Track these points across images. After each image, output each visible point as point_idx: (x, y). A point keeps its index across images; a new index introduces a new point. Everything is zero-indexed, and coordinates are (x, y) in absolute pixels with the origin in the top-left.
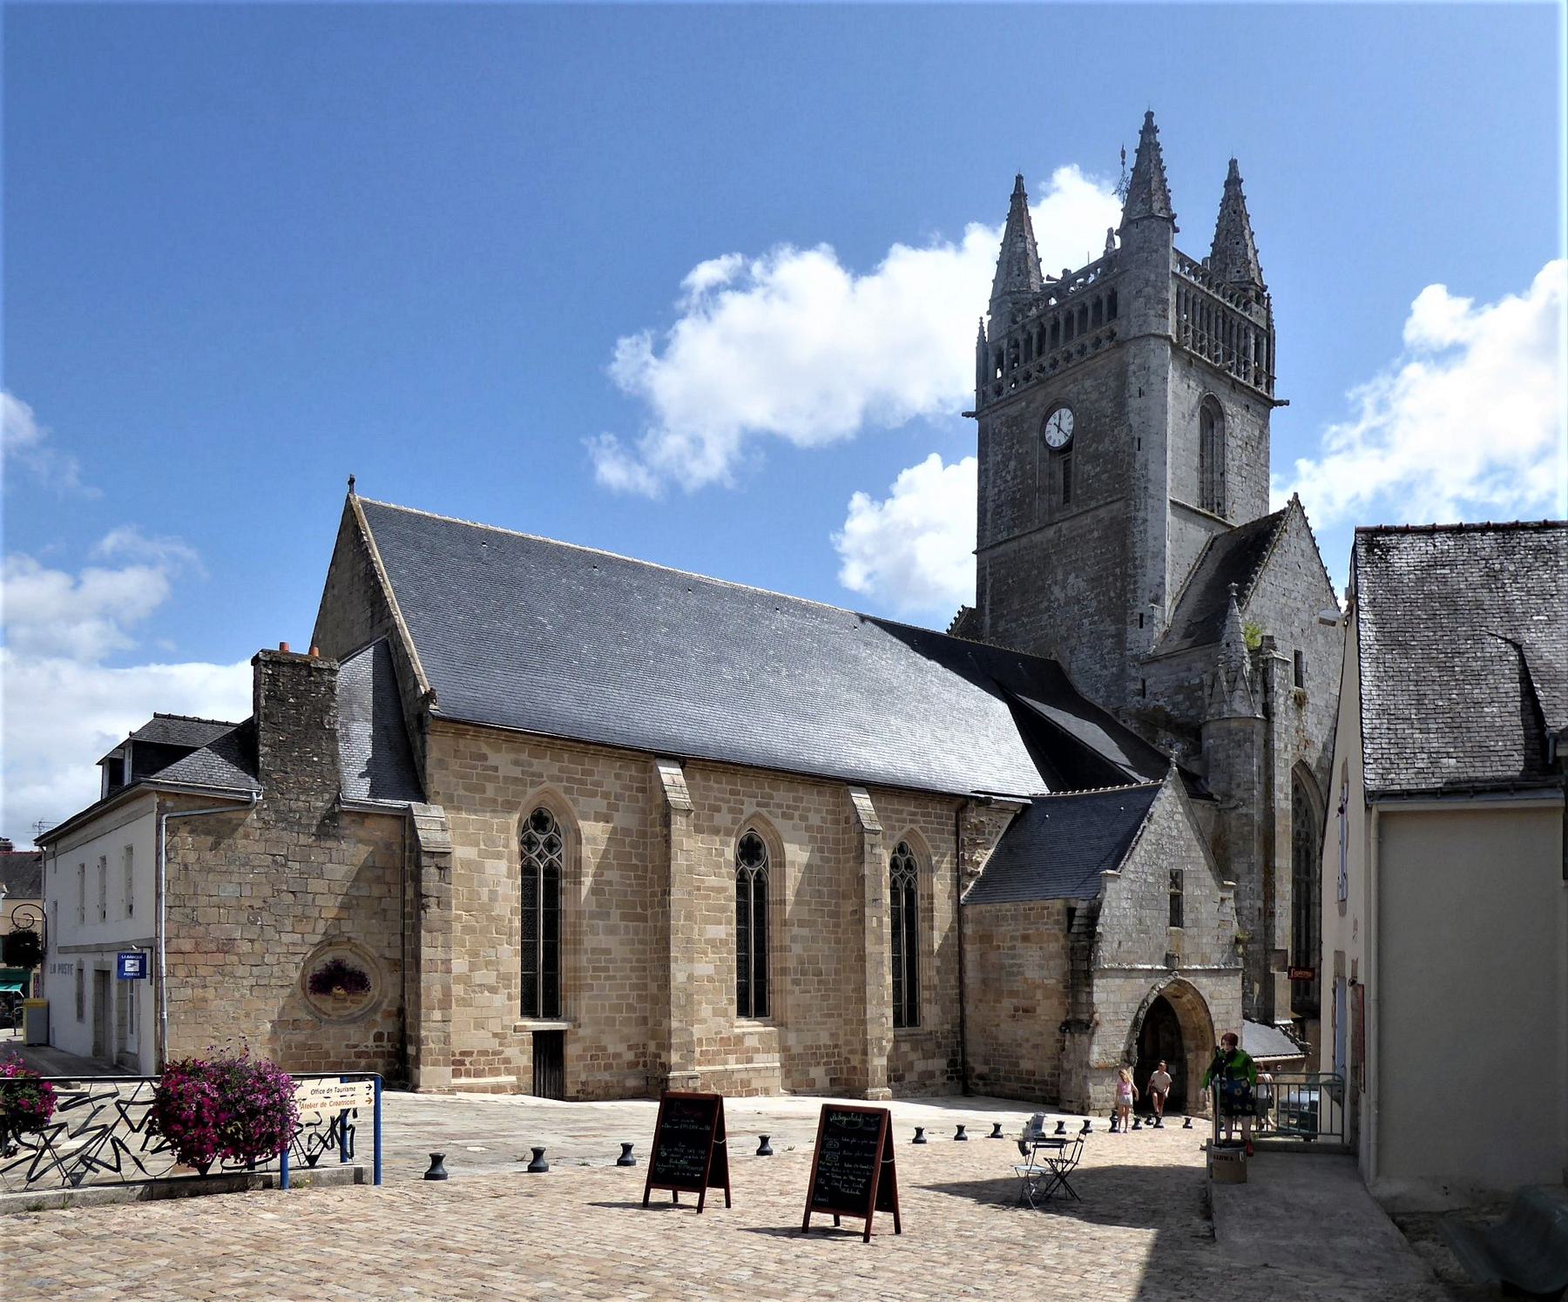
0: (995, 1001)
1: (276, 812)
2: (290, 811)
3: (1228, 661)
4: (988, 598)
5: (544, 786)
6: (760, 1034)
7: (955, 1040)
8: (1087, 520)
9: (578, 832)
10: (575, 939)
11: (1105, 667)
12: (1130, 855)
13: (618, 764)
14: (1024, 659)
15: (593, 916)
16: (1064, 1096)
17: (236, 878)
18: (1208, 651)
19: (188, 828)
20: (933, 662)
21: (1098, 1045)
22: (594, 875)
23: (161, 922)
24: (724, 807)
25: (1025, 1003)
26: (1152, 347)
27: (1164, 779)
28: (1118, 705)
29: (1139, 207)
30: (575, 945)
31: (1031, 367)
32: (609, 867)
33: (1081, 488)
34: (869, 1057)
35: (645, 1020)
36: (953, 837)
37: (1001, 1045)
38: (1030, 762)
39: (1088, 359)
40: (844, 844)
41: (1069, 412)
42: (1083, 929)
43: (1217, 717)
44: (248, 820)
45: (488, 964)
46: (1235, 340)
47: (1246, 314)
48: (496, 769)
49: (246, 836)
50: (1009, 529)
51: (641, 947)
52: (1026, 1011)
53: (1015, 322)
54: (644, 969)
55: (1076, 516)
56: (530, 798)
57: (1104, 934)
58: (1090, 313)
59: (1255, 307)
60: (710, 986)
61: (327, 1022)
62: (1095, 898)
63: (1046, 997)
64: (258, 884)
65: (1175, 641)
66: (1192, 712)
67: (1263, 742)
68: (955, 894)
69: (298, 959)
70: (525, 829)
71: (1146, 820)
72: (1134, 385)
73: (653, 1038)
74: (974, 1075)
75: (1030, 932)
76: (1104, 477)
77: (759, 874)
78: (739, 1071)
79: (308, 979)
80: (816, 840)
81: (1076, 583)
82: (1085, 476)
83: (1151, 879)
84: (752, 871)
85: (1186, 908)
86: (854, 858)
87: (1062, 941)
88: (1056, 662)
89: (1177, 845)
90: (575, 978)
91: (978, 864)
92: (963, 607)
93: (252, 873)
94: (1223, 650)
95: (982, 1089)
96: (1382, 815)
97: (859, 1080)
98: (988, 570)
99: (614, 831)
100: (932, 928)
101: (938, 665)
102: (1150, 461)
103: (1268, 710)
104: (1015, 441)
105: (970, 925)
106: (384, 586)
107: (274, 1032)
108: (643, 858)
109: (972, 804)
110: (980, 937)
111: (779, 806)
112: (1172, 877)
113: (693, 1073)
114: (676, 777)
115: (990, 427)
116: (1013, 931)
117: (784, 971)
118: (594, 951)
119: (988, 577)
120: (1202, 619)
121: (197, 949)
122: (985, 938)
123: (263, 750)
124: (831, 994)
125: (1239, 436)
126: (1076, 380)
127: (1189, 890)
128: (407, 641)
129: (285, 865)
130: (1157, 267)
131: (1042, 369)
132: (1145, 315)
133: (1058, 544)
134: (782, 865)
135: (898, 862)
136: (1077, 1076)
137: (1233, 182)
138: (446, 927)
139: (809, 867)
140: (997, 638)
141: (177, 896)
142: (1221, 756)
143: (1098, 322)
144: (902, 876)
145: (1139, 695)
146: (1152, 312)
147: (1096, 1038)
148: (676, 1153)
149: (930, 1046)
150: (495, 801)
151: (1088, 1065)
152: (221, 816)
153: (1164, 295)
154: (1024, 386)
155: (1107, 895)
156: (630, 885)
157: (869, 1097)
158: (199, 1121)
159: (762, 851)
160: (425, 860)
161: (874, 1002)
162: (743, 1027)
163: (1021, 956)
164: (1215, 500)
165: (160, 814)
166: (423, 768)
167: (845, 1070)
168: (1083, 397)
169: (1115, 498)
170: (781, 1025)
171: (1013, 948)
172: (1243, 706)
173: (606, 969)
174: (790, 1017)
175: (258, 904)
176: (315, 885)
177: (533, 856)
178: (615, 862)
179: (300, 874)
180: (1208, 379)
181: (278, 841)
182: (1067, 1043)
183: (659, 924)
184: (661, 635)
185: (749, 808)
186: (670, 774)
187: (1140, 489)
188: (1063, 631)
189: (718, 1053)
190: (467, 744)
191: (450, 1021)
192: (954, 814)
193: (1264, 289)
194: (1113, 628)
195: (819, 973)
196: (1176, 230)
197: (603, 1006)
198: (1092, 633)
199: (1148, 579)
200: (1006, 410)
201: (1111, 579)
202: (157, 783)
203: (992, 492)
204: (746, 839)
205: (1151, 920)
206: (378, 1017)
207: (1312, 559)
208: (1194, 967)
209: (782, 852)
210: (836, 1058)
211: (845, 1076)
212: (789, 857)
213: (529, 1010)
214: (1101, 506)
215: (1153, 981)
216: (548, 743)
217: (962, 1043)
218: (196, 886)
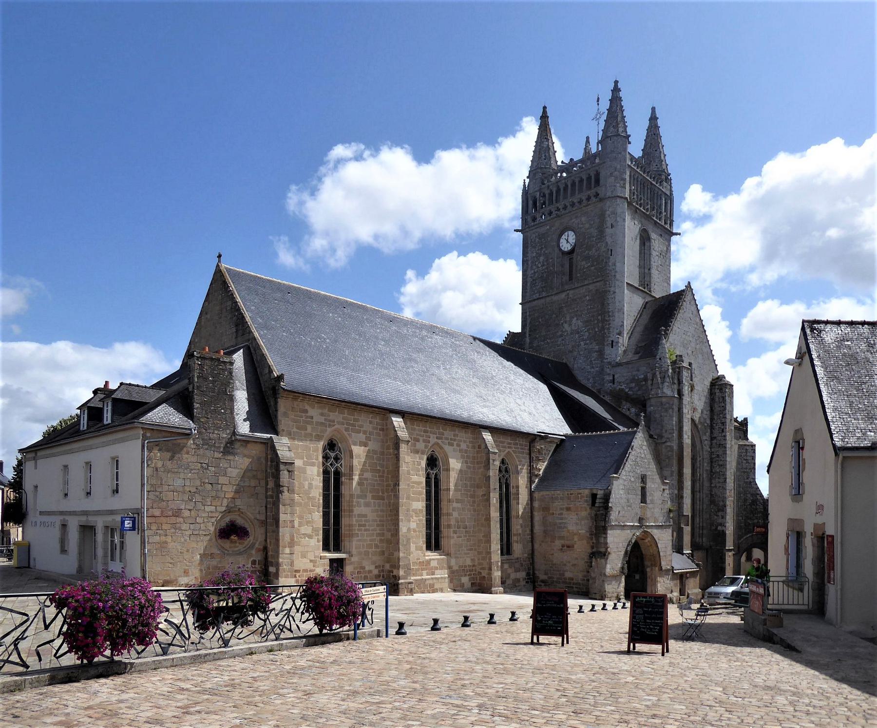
0: (551, 542)
1: (203, 439)
2: (210, 439)
4: (528, 328)
5: (336, 426)
6: (438, 559)
8: (583, 290)
9: (351, 452)
10: (350, 509)
11: (593, 367)
13: (371, 415)
15: (359, 497)
17: (182, 476)
19: (158, 448)
20: (509, 363)
22: (359, 475)
23: (144, 500)
25: (568, 543)
26: (618, 203)
27: (638, 428)
29: (612, 129)
30: (350, 512)
31: (552, 208)
32: (367, 471)
34: (493, 571)
35: (383, 553)
36: (528, 456)
37: (555, 564)
38: (561, 417)
39: (584, 206)
41: (573, 233)
42: (601, 505)
44: (189, 444)
45: (308, 522)
46: (655, 201)
47: (661, 188)
48: (312, 418)
49: (188, 453)
51: (381, 513)
52: (568, 547)
53: (543, 184)
54: (383, 525)
55: (577, 288)
56: (329, 433)
57: (613, 507)
58: (585, 182)
59: (665, 184)
61: (228, 554)
62: (607, 489)
64: (194, 479)
65: (630, 356)
66: (639, 393)
68: (529, 486)
69: (213, 520)
70: (324, 450)
72: (609, 221)
73: (388, 562)
75: (571, 506)
77: (436, 475)
78: (429, 579)
79: (217, 531)
80: (464, 457)
81: (577, 323)
83: (633, 479)
84: (433, 473)
85: (648, 494)
86: (484, 466)
88: (566, 364)
90: (350, 530)
91: (540, 470)
92: (509, 331)
93: (191, 473)
94: (657, 361)
96: (844, 457)
98: (528, 314)
99: (369, 451)
100: (518, 504)
101: (512, 364)
103: (680, 393)
105: (537, 502)
106: (245, 316)
107: (201, 560)
108: (382, 466)
109: (538, 439)
110: (543, 508)
111: (447, 439)
112: (642, 478)
113: (410, 581)
115: (529, 239)
117: (449, 526)
118: (359, 515)
119: (528, 317)
120: (643, 344)
121: (162, 515)
122: (546, 509)
123: (196, 405)
127: (649, 485)
128: (262, 347)
129: (207, 469)
130: (621, 161)
131: (558, 210)
133: (567, 302)
136: (599, 580)
137: (653, 119)
138: (292, 504)
139: (461, 471)
140: (533, 349)
141: (152, 485)
142: (657, 416)
146: (618, 185)
147: (608, 561)
148: (546, 618)
149: (517, 565)
150: (311, 435)
151: (605, 574)
152: (175, 442)
154: (549, 218)
155: (614, 487)
156: (377, 480)
158: (330, 607)
159: (438, 463)
160: (282, 467)
163: (566, 518)
164: (646, 283)
165: (143, 441)
166: (276, 417)
167: (478, 578)
168: (580, 226)
169: (598, 279)
171: (561, 514)
172: (668, 391)
173: (364, 525)
174: (452, 551)
175: (193, 490)
176: (222, 480)
177: (328, 464)
178: (369, 468)
179: (215, 473)
180: (643, 220)
181: (204, 456)
182: (593, 563)
183: (392, 501)
184: (381, 346)
185: (433, 440)
186: (397, 421)
188: (570, 347)
189: (417, 570)
190: (299, 404)
191: (293, 554)
193: (669, 175)
194: (597, 347)
196: (630, 143)
197: (363, 545)
200: (538, 230)
201: (596, 322)
202: (143, 423)
203: (530, 272)
206: (253, 552)
207: (696, 316)
208: (651, 524)
209: (448, 463)
211: (478, 581)
212: (452, 466)
213: (326, 548)
214: (590, 283)
215: (634, 531)
216: (338, 404)
217: (533, 563)
218: (162, 480)
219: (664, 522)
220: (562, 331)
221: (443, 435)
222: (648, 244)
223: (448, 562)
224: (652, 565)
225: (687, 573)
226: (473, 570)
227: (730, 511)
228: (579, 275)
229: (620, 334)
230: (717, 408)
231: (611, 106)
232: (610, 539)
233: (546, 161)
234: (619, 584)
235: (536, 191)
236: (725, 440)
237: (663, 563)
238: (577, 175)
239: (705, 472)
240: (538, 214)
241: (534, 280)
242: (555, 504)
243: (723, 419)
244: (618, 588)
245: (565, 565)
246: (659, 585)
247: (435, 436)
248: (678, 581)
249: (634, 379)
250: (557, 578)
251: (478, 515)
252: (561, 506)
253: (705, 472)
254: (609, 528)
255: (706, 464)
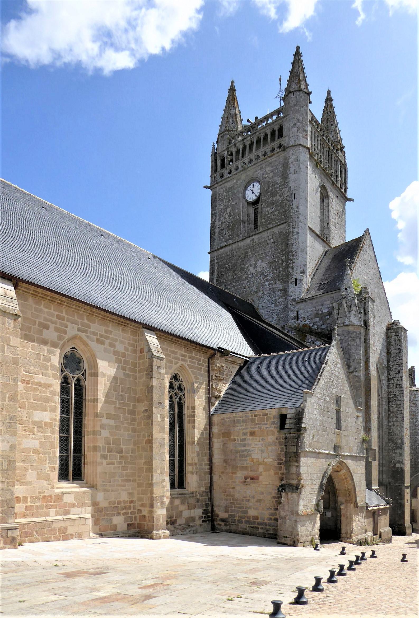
0: (232, 473)
3: (347, 296)
4: (216, 274)
6: (76, 493)
7: (207, 497)
11: (277, 306)
12: (318, 382)
14: (237, 299)
16: (281, 533)
18: (332, 295)
21: (303, 500)
24: (52, 326)
25: (252, 474)
28: (284, 324)
33: (264, 219)
34: (155, 509)
36: (207, 374)
37: (237, 500)
40: (139, 367)
41: (258, 184)
42: (293, 426)
43: (342, 325)
50: (227, 240)
52: (252, 479)
55: (262, 232)
60: (36, 457)
63: (265, 470)
67: (364, 340)
68: (207, 408)
71: (324, 364)
74: (218, 519)
75: (256, 430)
76: (276, 213)
77: (78, 380)
78: (58, 521)
81: (262, 265)
82: (267, 213)
83: (327, 399)
85: (343, 419)
86: (146, 375)
87: (276, 435)
89: (338, 381)
91: (220, 391)
95: (224, 528)
97: (147, 525)
98: (216, 261)
100: (194, 427)
102: (300, 204)
104: (230, 199)
105: (216, 426)
109: (218, 355)
113: (13, 525)
114: (8, 292)
116: (244, 429)
117: (95, 449)
119: (216, 264)
122: (226, 435)
124: (129, 466)
125: (335, 209)
126: (261, 168)
127: (344, 409)
132: (298, 136)
134: (95, 375)
135: (174, 385)
136: (290, 520)
139: (115, 378)
143: (273, 139)
144: (176, 394)
145: (295, 319)
146: (301, 135)
147: (302, 496)
149: (192, 501)
151: (297, 514)
153: (306, 128)
155: (307, 404)
157: (154, 537)
159: (81, 365)
161: (159, 472)
162: (63, 488)
163: (249, 445)
167: (138, 518)
169: (282, 222)
170: (92, 487)
171: (244, 440)
174: (99, 481)
180: (323, 177)
182: (283, 499)
185: (72, 331)
187: (295, 217)
189: (41, 507)
192: (207, 360)
194: (281, 286)
195: (121, 451)
198: (270, 289)
199: (298, 262)
200: (226, 185)
201: (280, 262)
204: (69, 353)
205: (327, 424)
208: (347, 454)
209: (95, 366)
210: (132, 510)
211: (138, 522)
212: (101, 370)
214: (274, 227)
215: (329, 461)
217: (211, 499)
219: (359, 453)
220: (247, 274)
221: (89, 327)
222: (327, 201)
223: (93, 497)
224: (346, 501)
225: (379, 510)
226: (130, 507)
227: (407, 448)
228: (263, 221)
229: (303, 272)
230: (393, 351)
231: (293, 67)
232: (303, 469)
233: (233, 125)
234: (314, 525)
235: (224, 151)
236: (402, 380)
237: (358, 499)
238: (262, 131)
239: (383, 411)
240: (225, 170)
241: (221, 230)
242: (236, 429)
243: (400, 361)
244: (312, 530)
245: (248, 500)
246: (354, 524)
247: (76, 326)
248: (372, 519)
249: (317, 314)
250: (240, 517)
251: (139, 436)
252: (244, 431)
253: (383, 411)
254: (302, 454)
255: (384, 403)
